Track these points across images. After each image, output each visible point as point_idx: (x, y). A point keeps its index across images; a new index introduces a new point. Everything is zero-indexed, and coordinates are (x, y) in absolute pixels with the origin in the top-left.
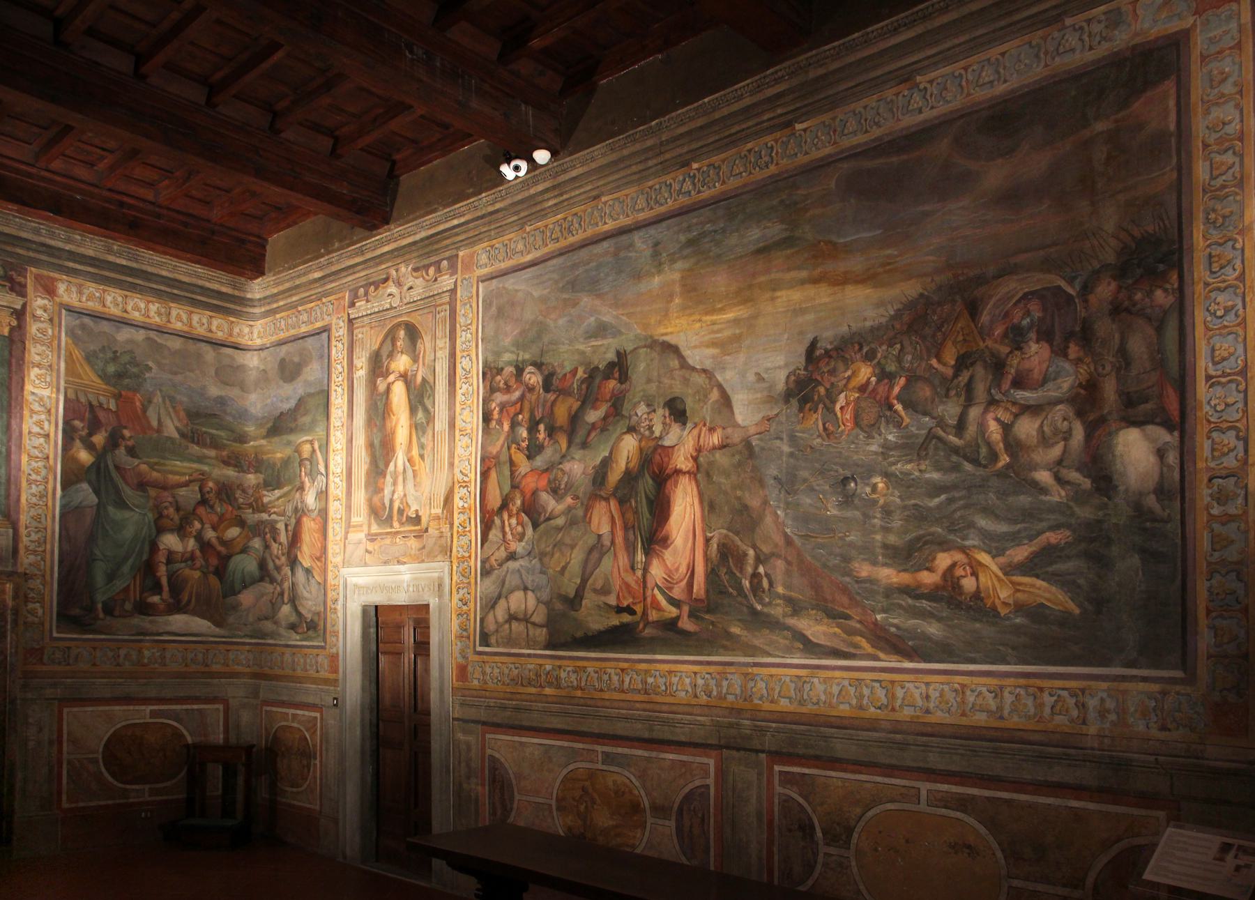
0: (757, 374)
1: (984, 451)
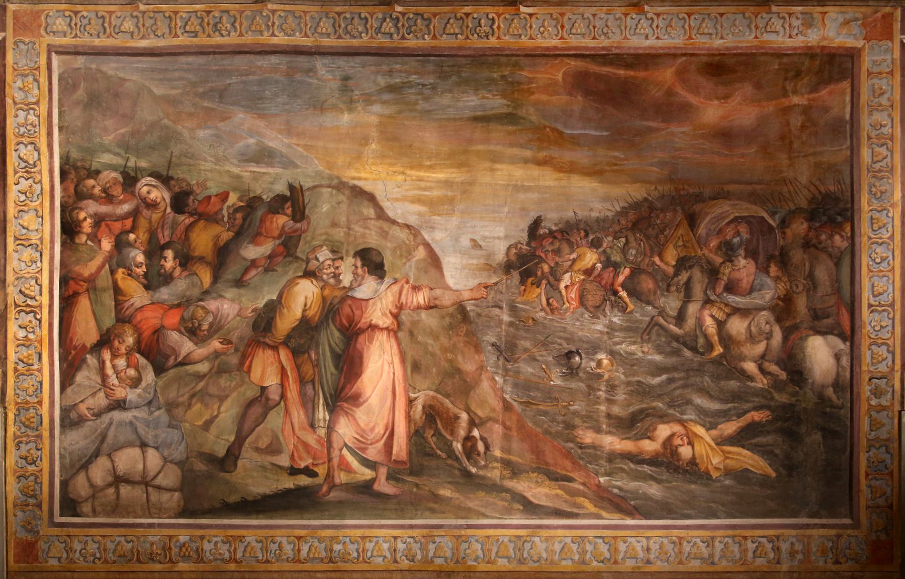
0: (473, 240)
1: (701, 341)
